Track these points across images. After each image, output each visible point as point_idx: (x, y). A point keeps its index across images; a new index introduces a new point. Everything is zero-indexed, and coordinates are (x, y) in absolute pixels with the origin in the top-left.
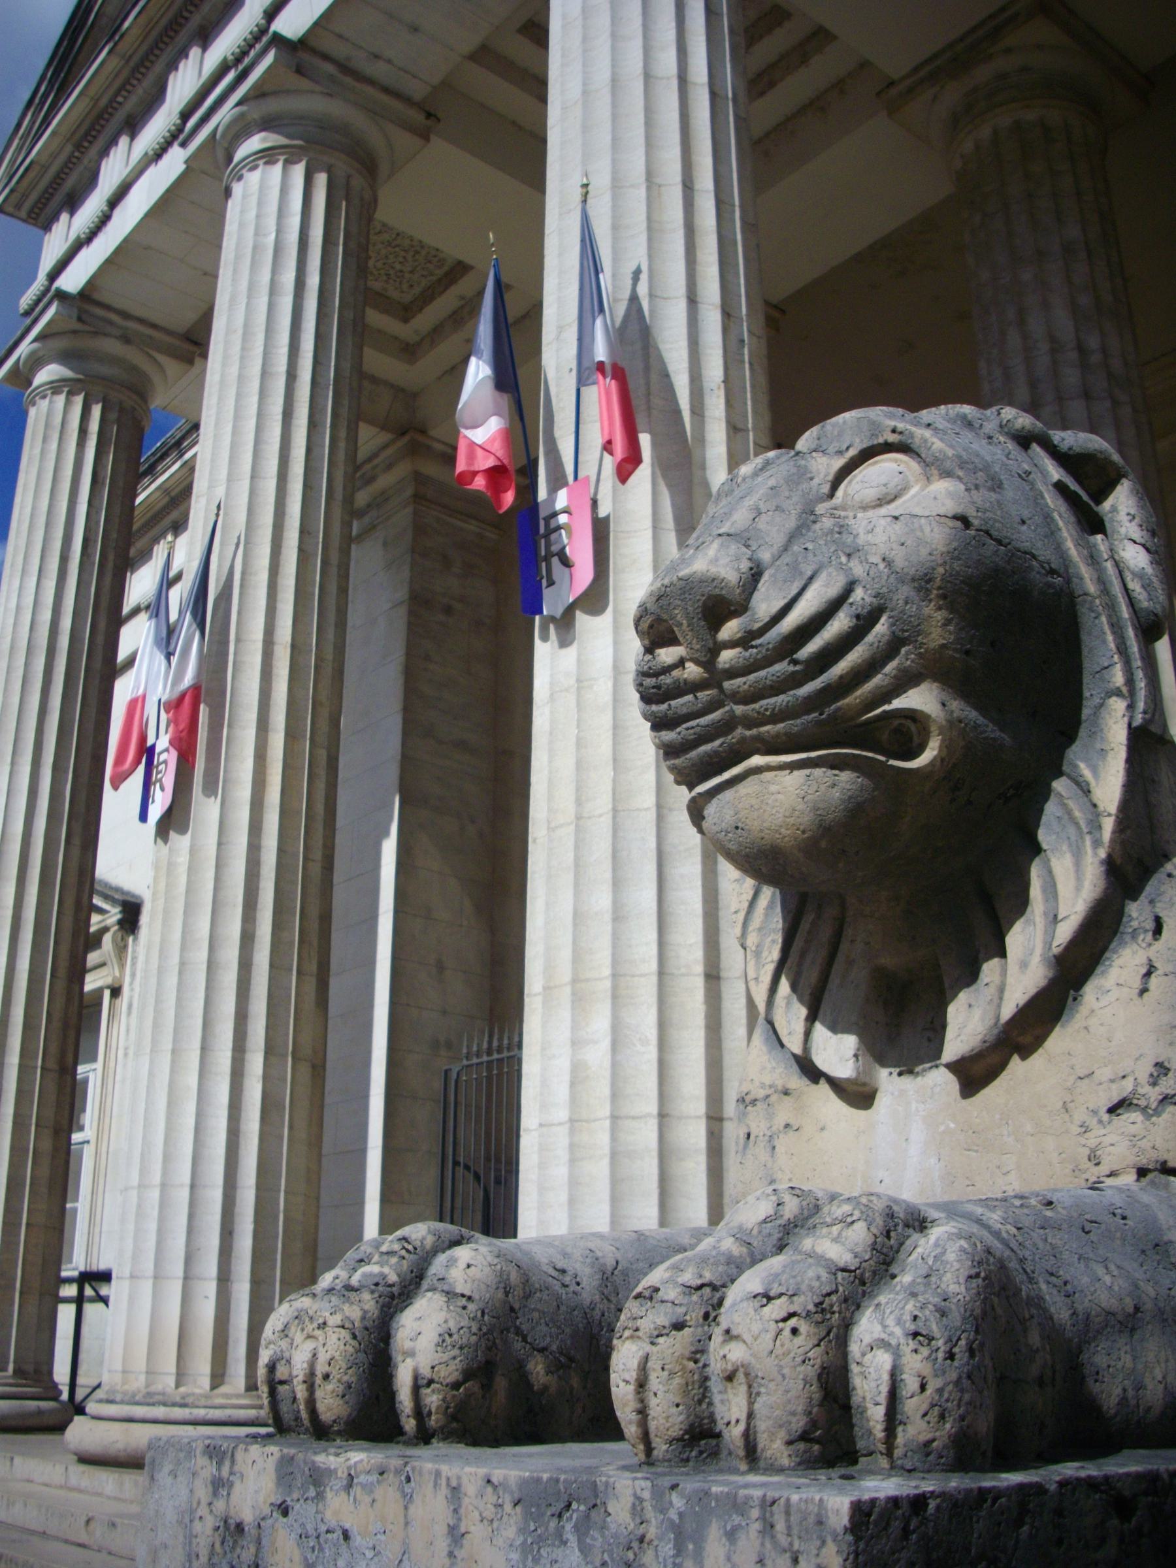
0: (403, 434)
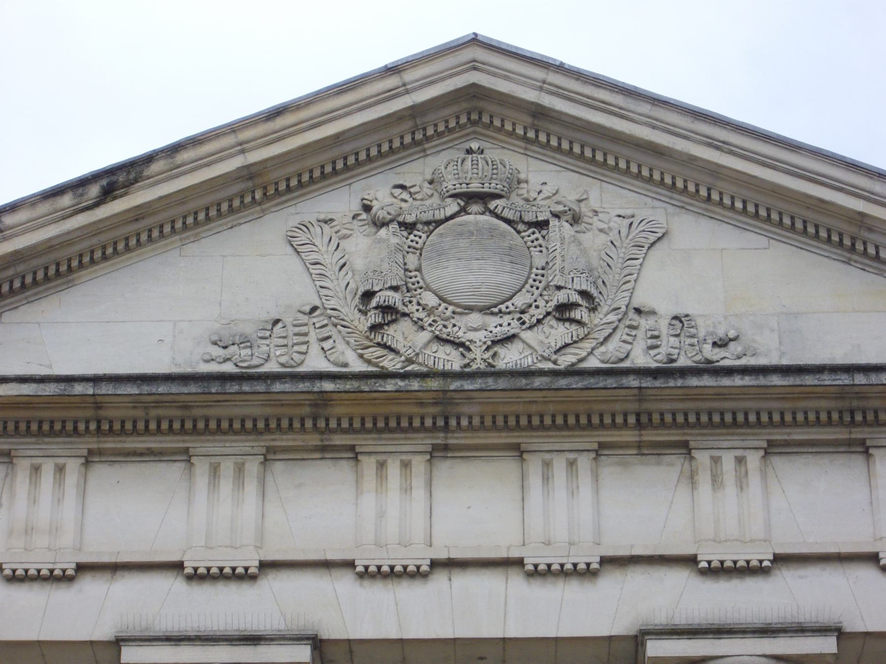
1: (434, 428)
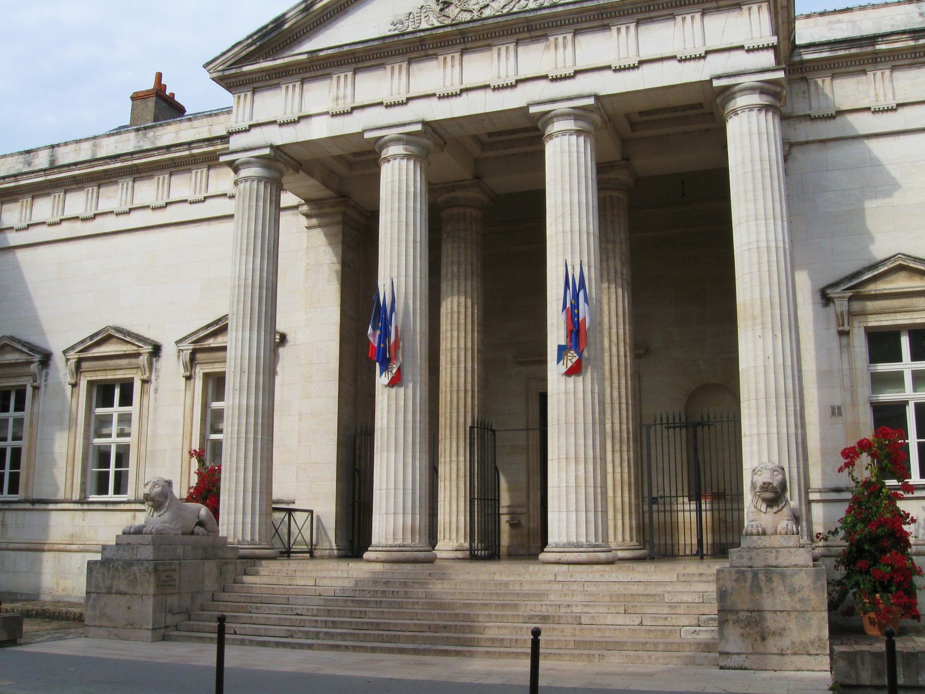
0: (343, 197)
1: (460, 43)
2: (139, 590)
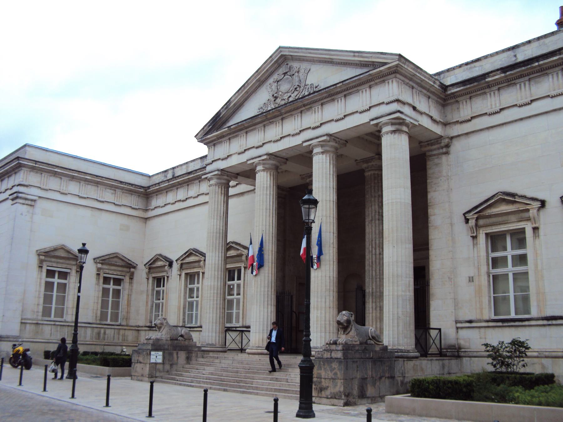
2: (145, 362)
